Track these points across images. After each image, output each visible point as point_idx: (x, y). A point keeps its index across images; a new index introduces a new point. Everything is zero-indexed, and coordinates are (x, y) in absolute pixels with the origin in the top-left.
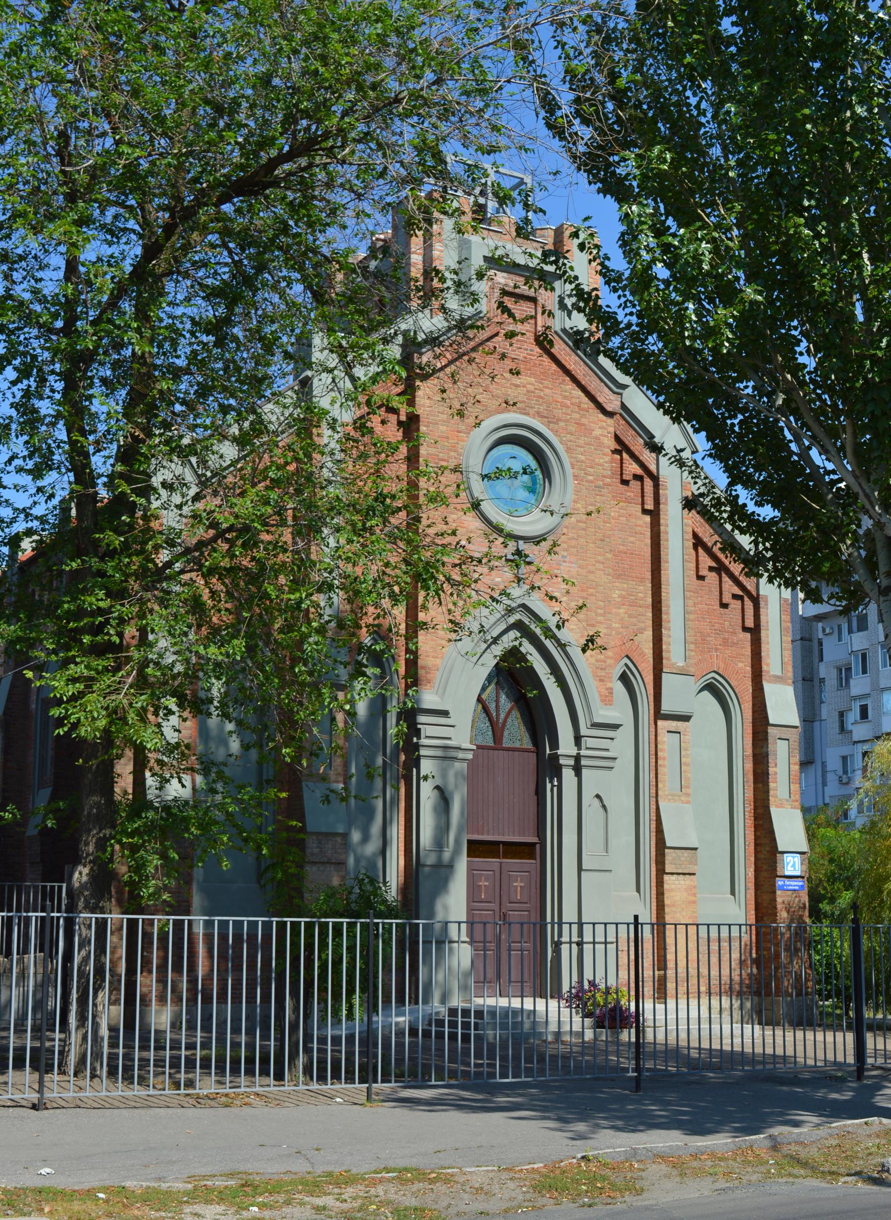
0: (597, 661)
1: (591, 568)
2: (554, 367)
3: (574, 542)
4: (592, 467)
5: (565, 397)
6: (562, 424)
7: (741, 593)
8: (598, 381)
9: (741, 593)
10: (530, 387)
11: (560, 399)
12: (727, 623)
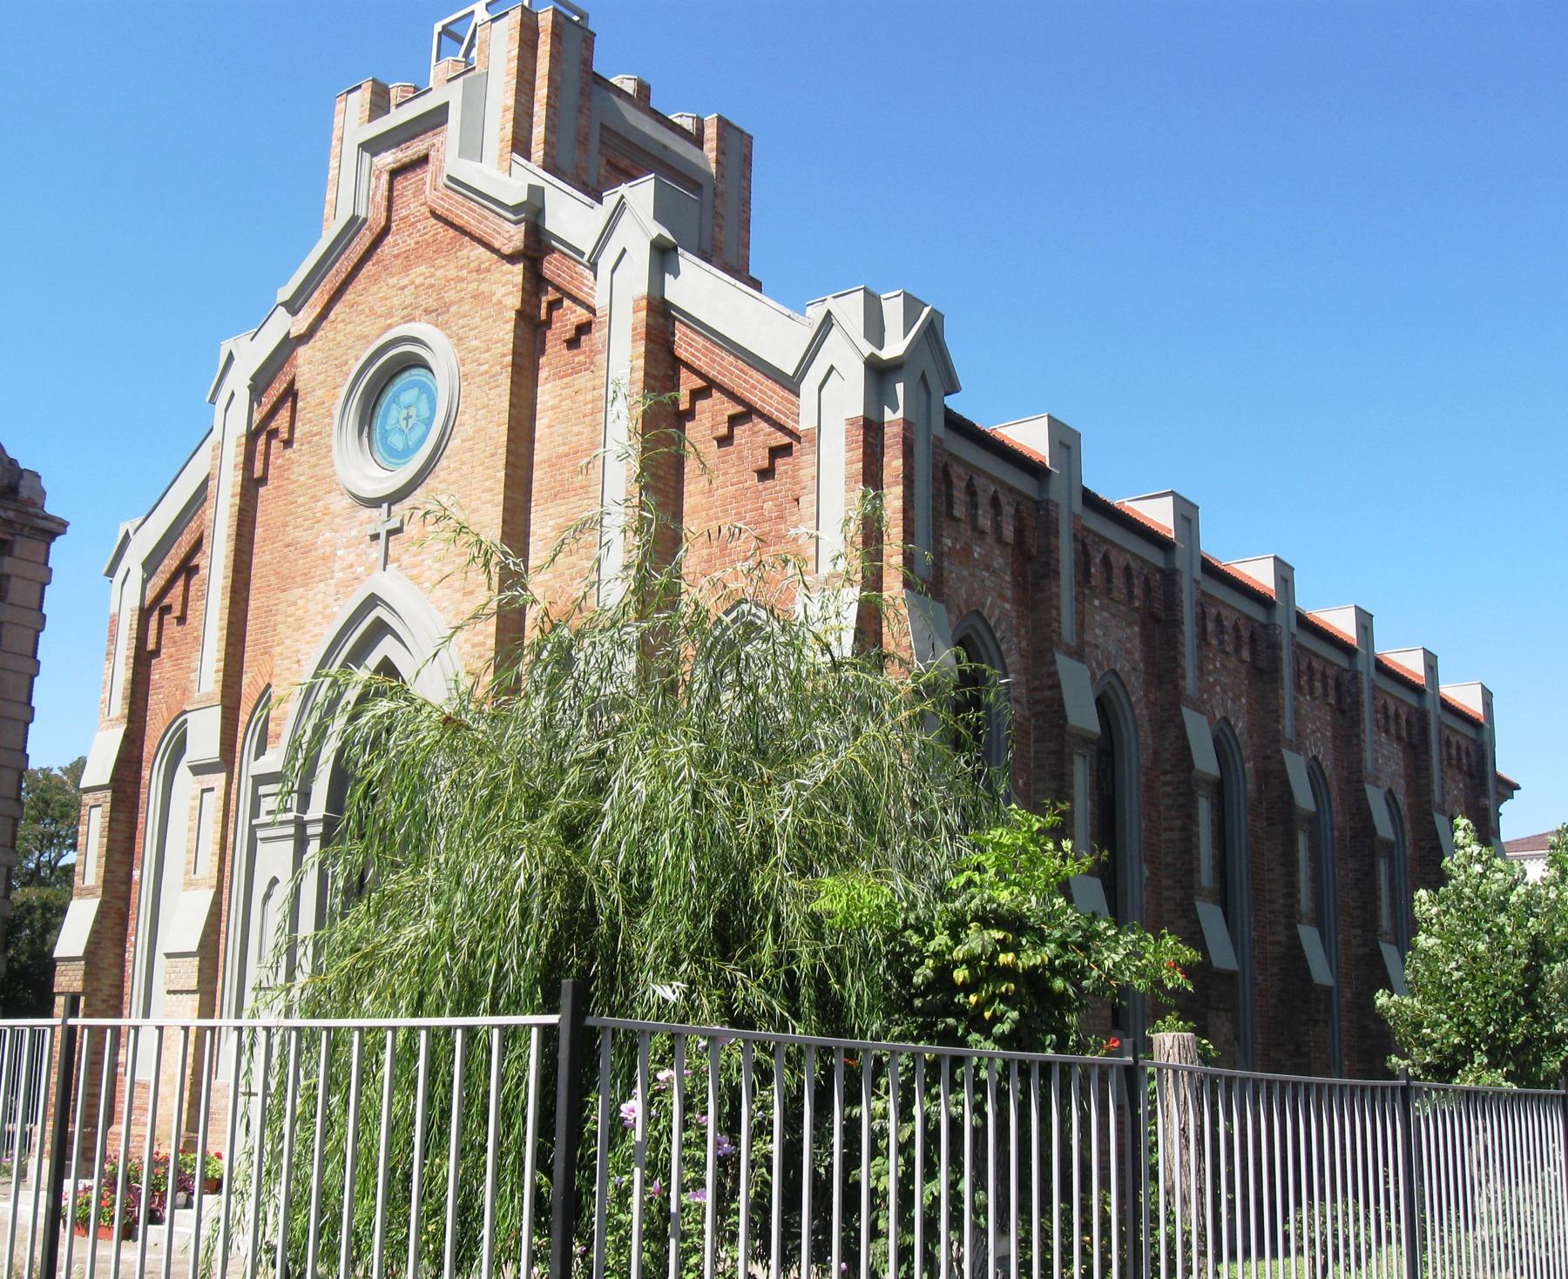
1: (474, 505)
2: (451, 232)
4: (488, 350)
6: (453, 309)
7: (787, 440)
10: (419, 280)
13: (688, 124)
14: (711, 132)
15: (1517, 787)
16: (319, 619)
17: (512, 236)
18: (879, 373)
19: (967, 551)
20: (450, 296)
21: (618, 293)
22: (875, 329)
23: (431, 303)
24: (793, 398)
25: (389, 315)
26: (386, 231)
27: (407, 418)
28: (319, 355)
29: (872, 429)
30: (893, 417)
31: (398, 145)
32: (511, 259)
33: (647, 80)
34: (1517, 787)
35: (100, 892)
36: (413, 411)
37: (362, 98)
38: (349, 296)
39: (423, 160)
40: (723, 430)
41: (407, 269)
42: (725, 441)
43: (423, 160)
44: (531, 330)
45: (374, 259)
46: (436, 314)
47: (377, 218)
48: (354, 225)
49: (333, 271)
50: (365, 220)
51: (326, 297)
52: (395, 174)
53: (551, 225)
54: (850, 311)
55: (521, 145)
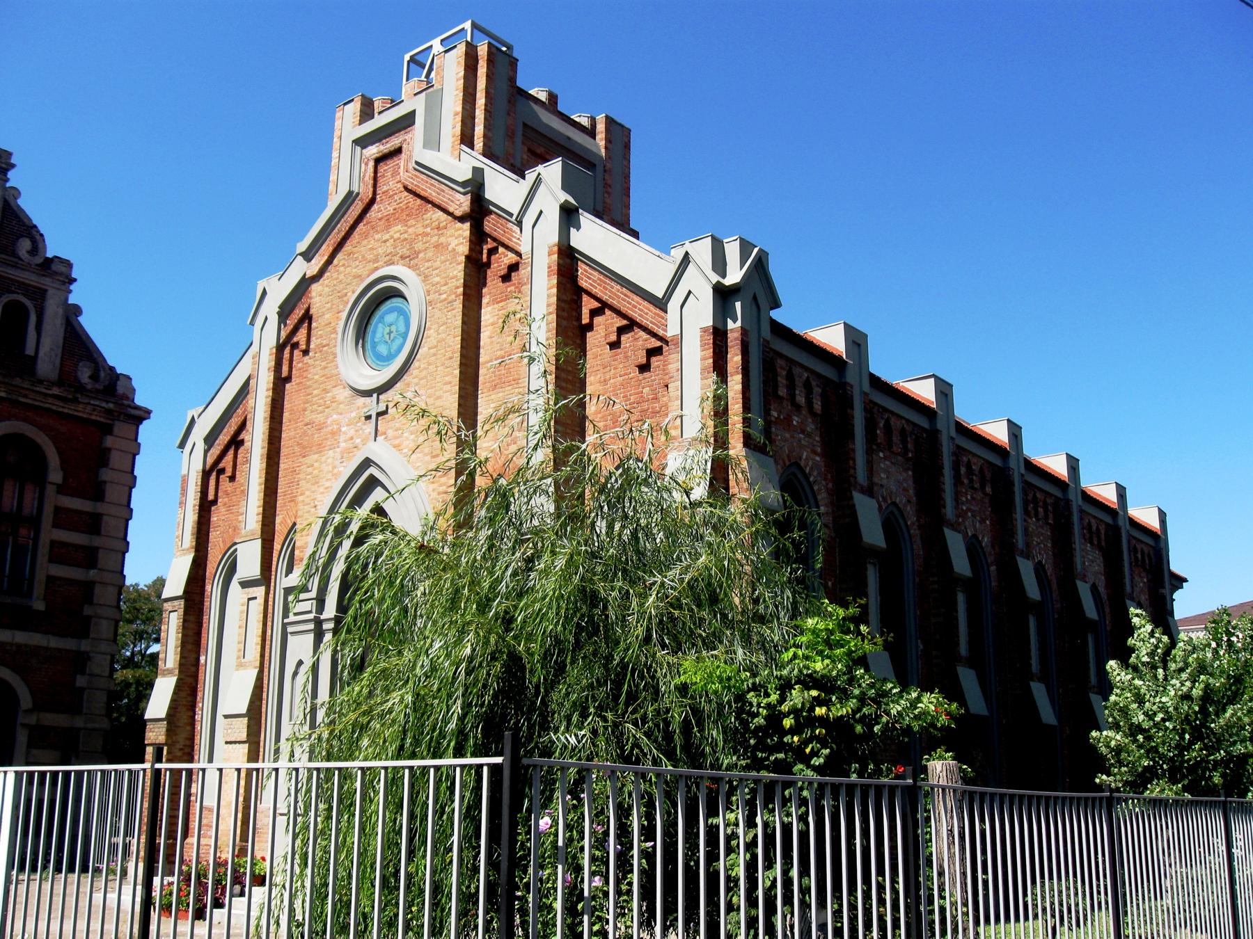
0: (439, 494)
2: (419, 201)
3: (424, 373)
5: (426, 226)
8: (451, 192)
9: (659, 344)
10: (396, 236)
11: (420, 230)
12: (646, 390)
13: (585, 121)
14: (601, 127)
15: (1186, 580)
16: (329, 476)
17: (462, 203)
18: (723, 296)
19: (788, 419)
20: (419, 246)
21: (538, 242)
22: (719, 264)
23: (405, 251)
24: (663, 314)
25: (376, 261)
26: (372, 201)
27: (390, 333)
28: (327, 289)
29: (719, 336)
30: (733, 326)
31: (380, 141)
32: (461, 219)
33: (555, 91)
34: (1186, 580)
35: (177, 672)
36: (393, 328)
37: (354, 108)
38: (348, 247)
39: (398, 151)
40: (613, 338)
41: (388, 228)
42: (615, 345)
43: (398, 151)
44: (476, 269)
45: (365, 221)
46: (409, 259)
47: (367, 192)
48: (350, 197)
49: (336, 230)
50: (358, 194)
51: (331, 249)
52: (379, 161)
53: (489, 195)
54: (702, 251)
55: (467, 139)
